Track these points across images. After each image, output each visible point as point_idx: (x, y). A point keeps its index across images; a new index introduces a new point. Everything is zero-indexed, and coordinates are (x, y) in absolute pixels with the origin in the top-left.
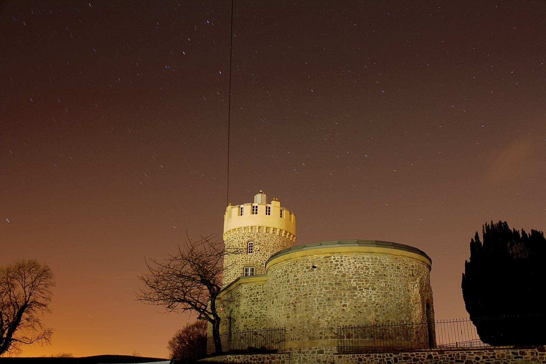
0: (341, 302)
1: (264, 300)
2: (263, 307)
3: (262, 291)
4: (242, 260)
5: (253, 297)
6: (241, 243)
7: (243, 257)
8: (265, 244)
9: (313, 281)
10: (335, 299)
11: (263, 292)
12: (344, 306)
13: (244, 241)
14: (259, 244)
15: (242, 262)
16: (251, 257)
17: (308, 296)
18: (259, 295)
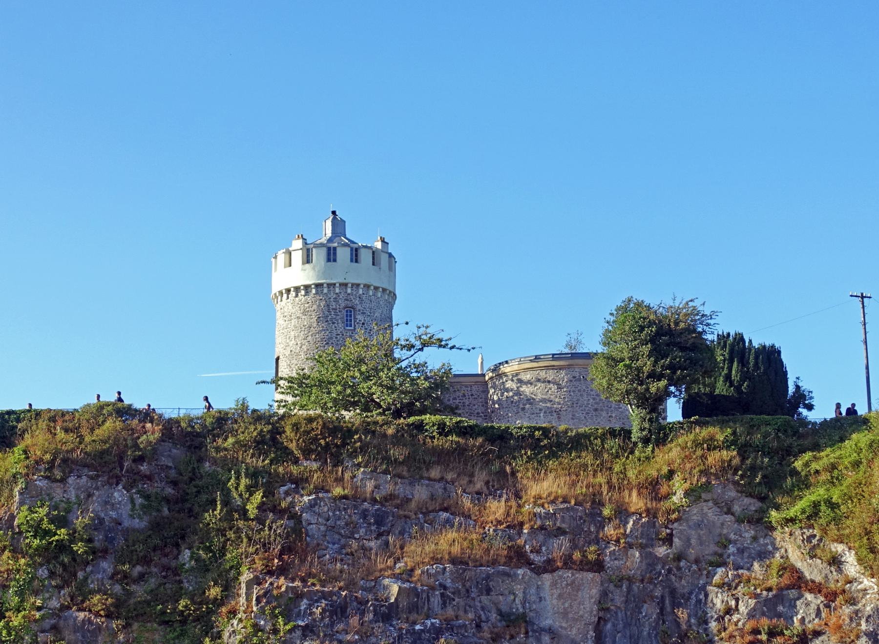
0: (608, 414)
1: (474, 405)
2: (473, 413)
3: (470, 394)
4: (336, 338)
5: (458, 401)
6: (333, 309)
7: (339, 333)
8: (370, 313)
9: (579, 391)
10: (602, 410)
11: (472, 395)
12: (610, 417)
13: (338, 307)
14: (364, 313)
15: (338, 341)
16: (352, 333)
17: (575, 405)
18: (466, 399)
